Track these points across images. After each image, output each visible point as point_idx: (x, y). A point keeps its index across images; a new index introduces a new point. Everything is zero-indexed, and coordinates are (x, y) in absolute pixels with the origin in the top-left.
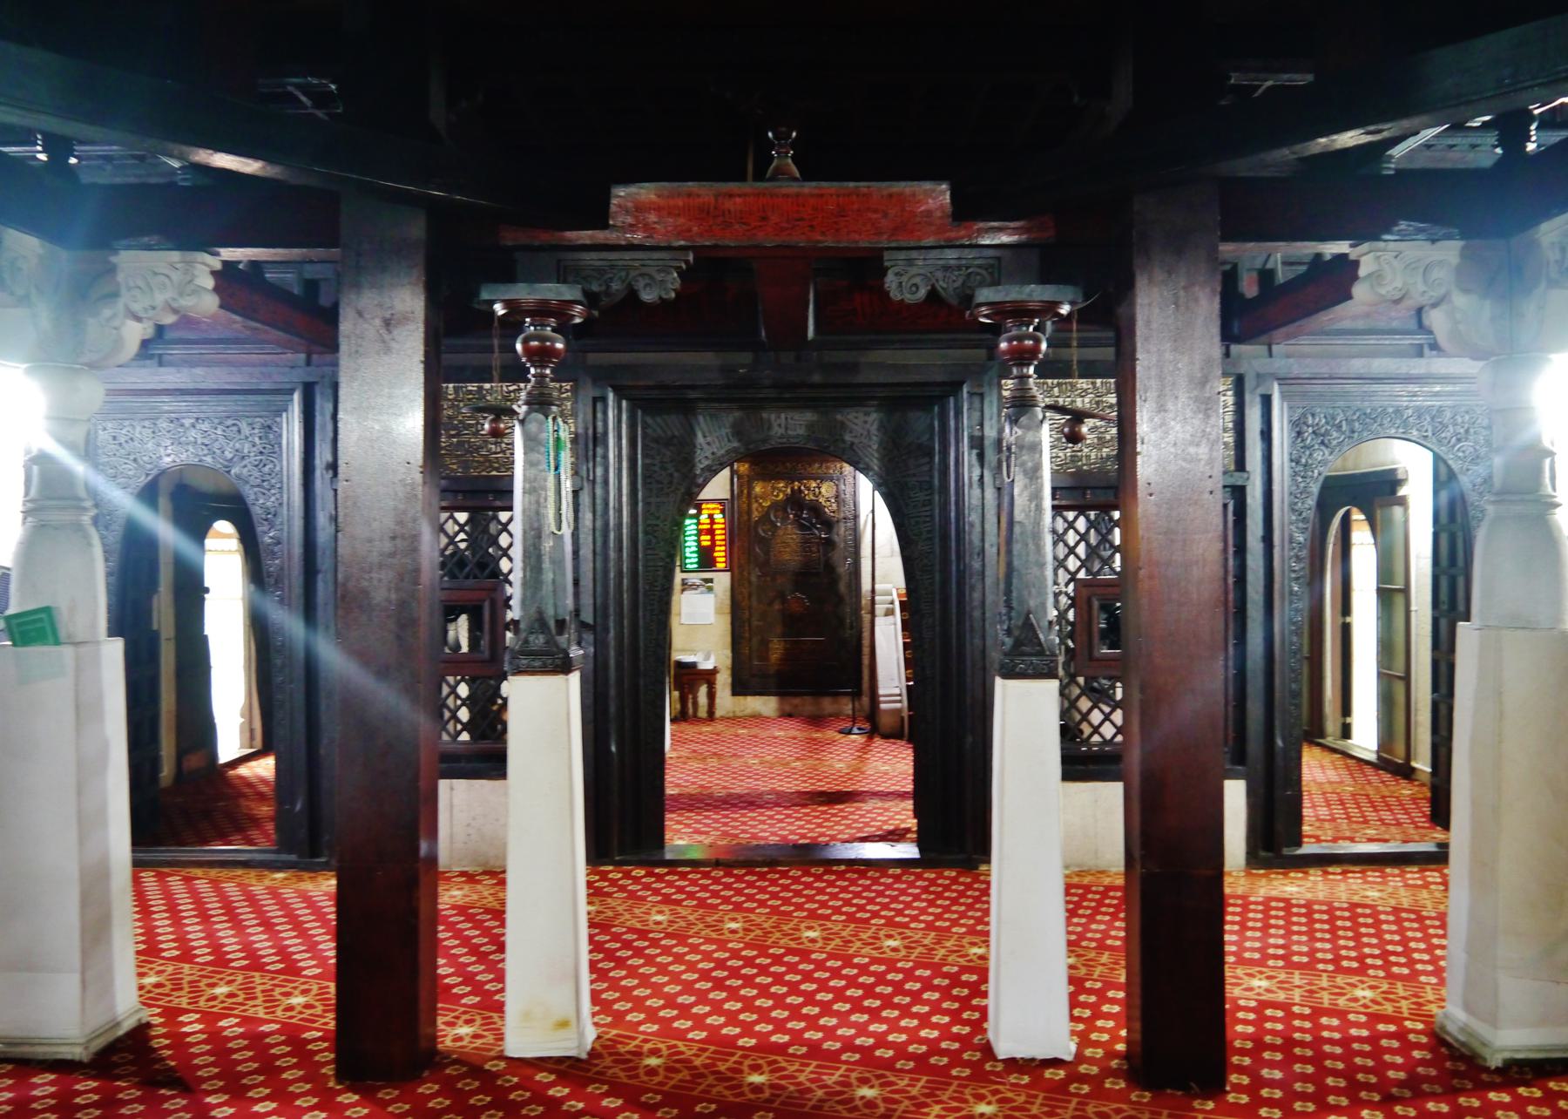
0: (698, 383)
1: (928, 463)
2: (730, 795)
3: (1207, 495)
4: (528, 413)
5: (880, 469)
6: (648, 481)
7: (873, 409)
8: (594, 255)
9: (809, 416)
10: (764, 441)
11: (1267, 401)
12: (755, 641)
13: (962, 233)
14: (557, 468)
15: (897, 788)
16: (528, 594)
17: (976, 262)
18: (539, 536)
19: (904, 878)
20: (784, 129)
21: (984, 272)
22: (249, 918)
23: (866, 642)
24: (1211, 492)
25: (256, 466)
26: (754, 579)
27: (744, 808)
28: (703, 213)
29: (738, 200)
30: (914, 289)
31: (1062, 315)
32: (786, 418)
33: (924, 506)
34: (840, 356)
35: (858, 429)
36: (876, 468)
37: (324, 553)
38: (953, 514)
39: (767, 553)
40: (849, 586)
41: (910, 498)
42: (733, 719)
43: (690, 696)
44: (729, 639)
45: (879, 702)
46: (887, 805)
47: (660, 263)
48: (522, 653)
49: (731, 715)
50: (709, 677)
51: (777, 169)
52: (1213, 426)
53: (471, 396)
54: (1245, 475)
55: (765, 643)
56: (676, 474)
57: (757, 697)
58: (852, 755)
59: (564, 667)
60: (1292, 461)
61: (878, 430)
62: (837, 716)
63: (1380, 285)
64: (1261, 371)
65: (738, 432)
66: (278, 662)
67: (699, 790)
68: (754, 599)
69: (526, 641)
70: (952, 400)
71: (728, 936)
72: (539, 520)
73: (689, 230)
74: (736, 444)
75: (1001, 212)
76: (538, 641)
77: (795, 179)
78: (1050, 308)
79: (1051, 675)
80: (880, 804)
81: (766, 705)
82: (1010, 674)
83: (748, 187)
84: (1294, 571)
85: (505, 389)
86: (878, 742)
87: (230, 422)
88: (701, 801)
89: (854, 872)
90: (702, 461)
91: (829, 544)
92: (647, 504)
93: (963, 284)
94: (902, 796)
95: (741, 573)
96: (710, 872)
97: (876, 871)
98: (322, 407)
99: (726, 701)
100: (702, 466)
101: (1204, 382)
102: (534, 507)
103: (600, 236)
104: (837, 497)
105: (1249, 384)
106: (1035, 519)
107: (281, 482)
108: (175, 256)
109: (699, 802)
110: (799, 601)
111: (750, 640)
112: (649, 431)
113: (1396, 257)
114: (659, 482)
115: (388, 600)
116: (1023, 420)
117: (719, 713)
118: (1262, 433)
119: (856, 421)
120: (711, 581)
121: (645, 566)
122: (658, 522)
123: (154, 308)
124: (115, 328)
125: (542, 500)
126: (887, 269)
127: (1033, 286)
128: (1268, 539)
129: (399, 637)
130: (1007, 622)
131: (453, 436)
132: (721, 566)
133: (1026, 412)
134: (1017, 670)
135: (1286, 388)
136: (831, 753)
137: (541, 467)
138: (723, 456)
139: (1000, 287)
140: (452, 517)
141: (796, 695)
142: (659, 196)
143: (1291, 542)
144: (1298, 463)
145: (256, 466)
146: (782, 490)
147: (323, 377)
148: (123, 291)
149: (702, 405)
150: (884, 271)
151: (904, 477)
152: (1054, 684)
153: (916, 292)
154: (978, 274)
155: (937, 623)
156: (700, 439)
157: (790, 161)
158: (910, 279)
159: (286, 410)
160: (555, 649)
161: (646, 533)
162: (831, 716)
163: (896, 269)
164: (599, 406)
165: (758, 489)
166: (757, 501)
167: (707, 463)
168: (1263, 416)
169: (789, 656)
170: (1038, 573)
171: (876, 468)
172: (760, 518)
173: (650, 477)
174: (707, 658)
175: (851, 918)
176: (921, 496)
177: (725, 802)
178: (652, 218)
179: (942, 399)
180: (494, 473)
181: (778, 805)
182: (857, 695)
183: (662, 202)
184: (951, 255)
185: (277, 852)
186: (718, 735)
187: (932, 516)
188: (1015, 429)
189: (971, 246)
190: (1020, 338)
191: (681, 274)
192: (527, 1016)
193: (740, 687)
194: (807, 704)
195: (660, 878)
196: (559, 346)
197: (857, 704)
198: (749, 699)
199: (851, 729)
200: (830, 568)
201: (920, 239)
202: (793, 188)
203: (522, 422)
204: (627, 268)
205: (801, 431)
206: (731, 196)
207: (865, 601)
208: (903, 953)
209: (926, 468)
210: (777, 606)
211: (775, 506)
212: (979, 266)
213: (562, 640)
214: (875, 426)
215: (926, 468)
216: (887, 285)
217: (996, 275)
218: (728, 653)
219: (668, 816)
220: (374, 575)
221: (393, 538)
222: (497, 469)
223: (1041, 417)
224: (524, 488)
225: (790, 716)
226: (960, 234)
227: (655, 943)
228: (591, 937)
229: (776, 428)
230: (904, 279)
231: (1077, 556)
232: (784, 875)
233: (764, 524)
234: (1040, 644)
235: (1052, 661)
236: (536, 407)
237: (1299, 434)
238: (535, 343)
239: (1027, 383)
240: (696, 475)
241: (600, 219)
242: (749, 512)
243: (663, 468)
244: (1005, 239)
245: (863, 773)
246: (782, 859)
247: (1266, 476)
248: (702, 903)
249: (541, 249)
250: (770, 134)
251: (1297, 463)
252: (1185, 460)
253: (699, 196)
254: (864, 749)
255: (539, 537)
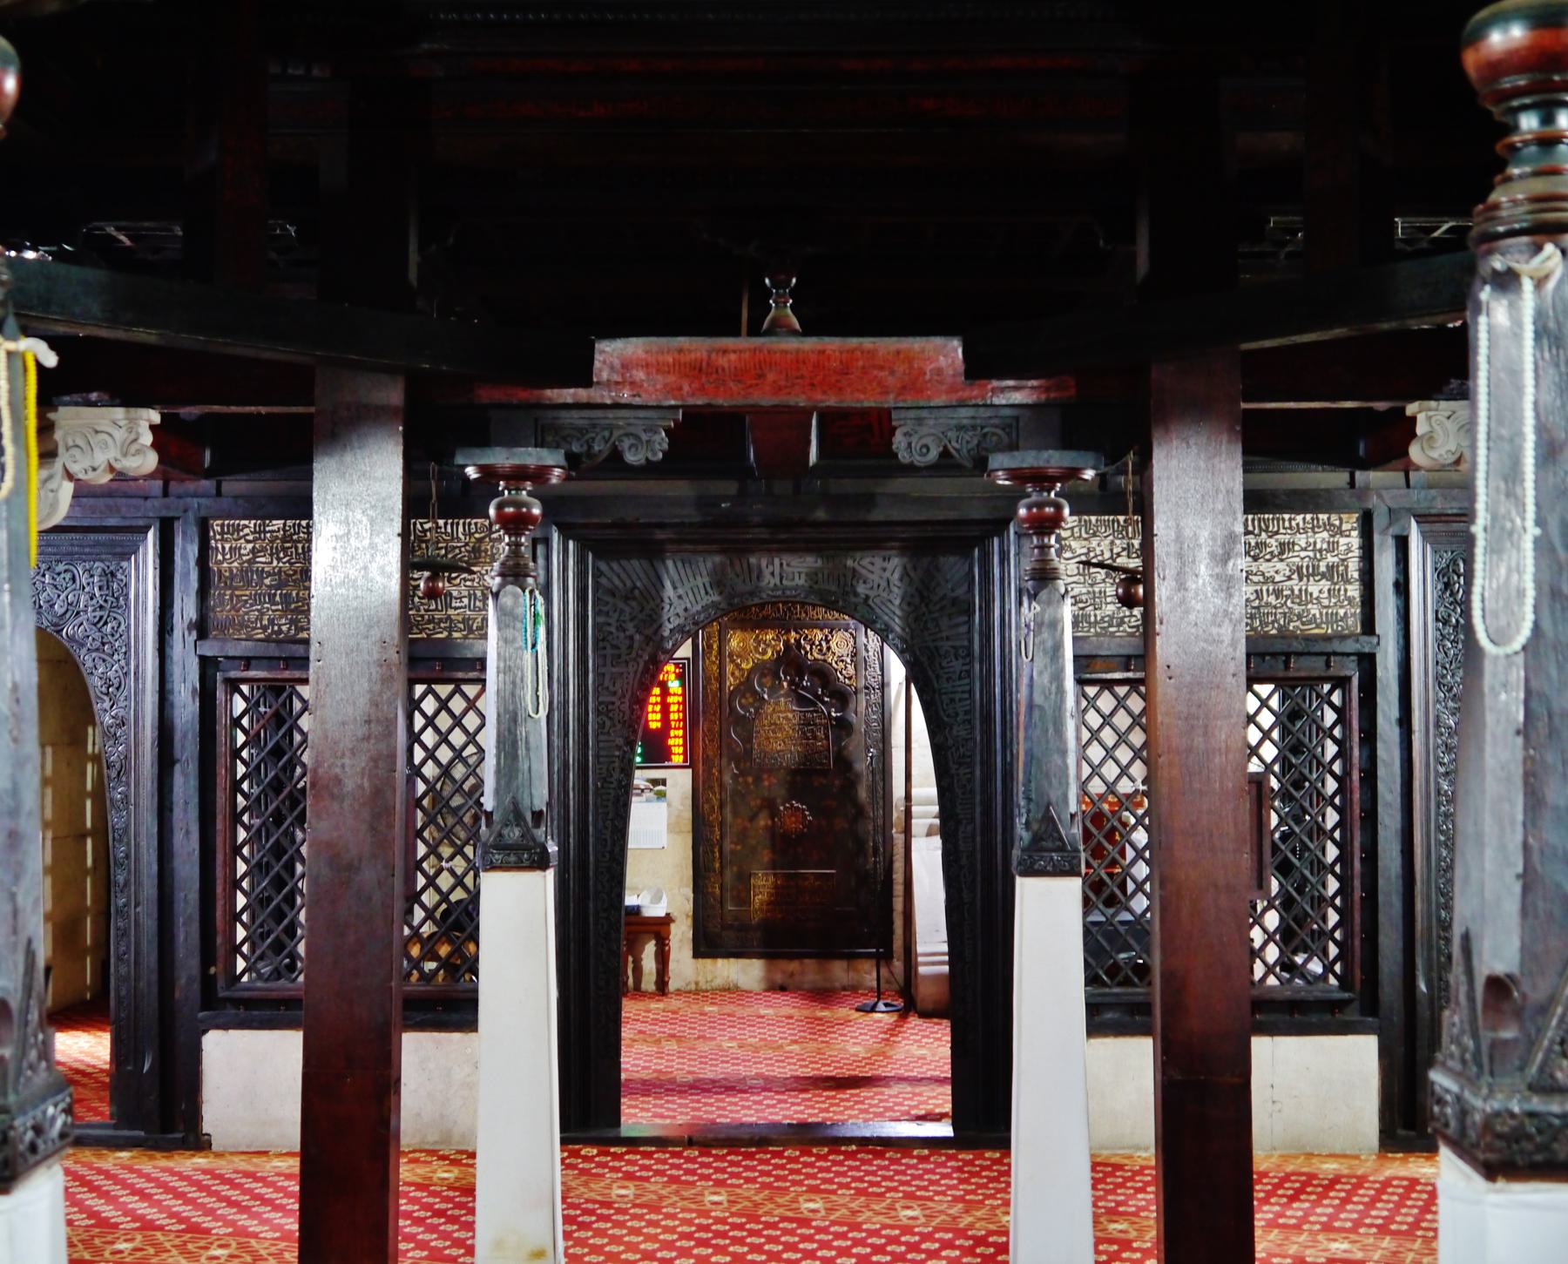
0: (667, 521)
1: (965, 623)
2: (700, 1080)
3: (1229, 679)
4: (502, 586)
5: (903, 629)
6: (601, 644)
7: (894, 552)
8: (575, 414)
9: (810, 562)
10: (752, 594)
11: (1402, 544)
12: (729, 875)
13: (975, 393)
14: (534, 646)
15: (937, 1073)
16: (503, 783)
17: (992, 422)
18: (514, 720)
19: (932, 1159)
20: (783, 277)
21: (1000, 432)
22: (117, 1190)
23: (898, 877)
24: (1234, 675)
25: (95, 625)
26: (727, 779)
27: (721, 1093)
28: (697, 370)
29: (733, 357)
30: (924, 450)
31: (1086, 480)
32: (781, 565)
33: (960, 678)
34: (848, 486)
35: (875, 578)
36: (898, 629)
38: (998, 690)
39: (748, 740)
40: (872, 790)
41: (942, 668)
42: (697, 993)
43: (630, 959)
44: (689, 872)
45: (917, 965)
46: (917, 1090)
47: (647, 422)
48: (496, 847)
49: (693, 987)
50: (659, 928)
51: (774, 322)
52: (1235, 606)
54: (1375, 640)
55: (744, 878)
56: (637, 637)
57: (732, 960)
58: (876, 1037)
59: (541, 863)
60: (1437, 619)
61: (901, 580)
62: (854, 989)
63: (1432, 448)
64: (1394, 506)
65: (718, 582)
66: (121, 879)
67: (655, 1075)
68: (728, 810)
69: (500, 835)
70: (996, 541)
71: (709, 1206)
72: (514, 703)
73: (680, 389)
74: (716, 598)
75: (1018, 371)
76: (514, 834)
77: (794, 333)
78: (1073, 473)
79: (1072, 872)
80: (909, 1089)
81: (746, 972)
82: (1025, 874)
83: (744, 343)
84: (1442, 764)
85: (418, 526)
86: (914, 1021)
87: (61, 567)
88: (655, 1086)
89: (869, 1152)
90: (671, 619)
91: (843, 726)
92: (599, 675)
93: (978, 445)
94: (939, 1081)
95: (708, 771)
96: (682, 1152)
97: (896, 1152)
98: (184, 550)
99: (684, 965)
100: (671, 626)
101: (1225, 558)
102: (509, 687)
103: (582, 394)
104: (854, 655)
105: (1379, 522)
106: (1055, 702)
107: (128, 645)
108: (119, 413)
109: (652, 1087)
110: (796, 815)
111: (721, 873)
112: (603, 581)
113: (1449, 418)
114: (616, 647)
115: (361, 787)
116: (1043, 595)
117: (673, 985)
118: (1397, 585)
119: (870, 567)
120: (663, 782)
121: (597, 756)
122: (613, 699)
123: (94, 469)
124: (52, 491)
125: (518, 681)
126: (895, 429)
127: (1051, 452)
128: (1405, 721)
129: (373, 828)
130: (1025, 816)
132: (677, 759)
133: (1045, 586)
134: (1036, 867)
135: (1427, 527)
136: (845, 1035)
137: (517, 645)
138: (698, 613)
139: (1016, 453)
141: (791, 957)
142: (647, 352)
143: (1437, 725)
144: (1446, 622)
145: (95, 625)
146: (770, 644)
147: (185, 511)
148: (61, 450)
149: (669, 547)
150: (893, 431)
151: (934, 641)
152: (1076, 883)
153: (925, 455)
154: (994, 434)
155: (978, 831)
156: (669, 591)
157: (789, 311)
158: (921, 438)
159: (135, 552)
160: (531, 843)
161: (598, 713)
162: (844, 989)
163: (904, 429)
164: (540, 549)
165: (735, 642)
166: (733, 661)
167: (676, 622)
168: (1398, 563)
169: (781, 897)
170: (1059, 762)
171: (898, 629)
172: (737, 688)
173: (603, 640)
174: (657, 899)
175: (860, 1192)
176: (957, 665)
177: (692, 1087)
178: (640, 375)
179: (983, 541)
181: (769, 1090)
182: (884, 957)
183: (652, 359)
184: (964, 413)
185: (115, 1127)
186: (674, 1012)
187: (971, 692)
188: (1034, 604)
189: (985, 406)
190: (1040, 505)
191: (668, 431)
192: (499, 1245)
193: (706, 945)
194: (808, 972)
195: (617, 1157)
196: (536, 511)
197: (884, 971)
198: (720, 962)
199: (875, 1005)
200: (844, 764)
201: (929, 399)
202: (792, 344)
203: (496, 595)
204: (611, 428)
205: (801, 581)
206: (725, 352)
207: (897, 813)
208: (923, 1220)
209: (963, 629)
210: (763, 821)
211: (759, 668)
212: (997, 426)
213: (540, 833)
214: (897, 575)
215: (963, 629)
216: (894, 447)
217: (1014, 435)
218: (689, 892)
219: (622, 1100)
220: (347, 761)
221: (368, 722)
223: (1062, 590)
224: (498, 668)
225: (783, 989)
226: (973, 393)
227: (620, 1211)
228: (563, 1160)
229: (767, 578)
230: (914, 440)
231: (423, 714)
232: (779, 1155)
233: (743, 696)
234: (1061, 838)
235: (1074, 858)
236: (510, 579)
237: (1447, 585)
238: (510, 510)
239: (1048, 554)
240: (663, 637)
241: (586, 380)
242: (721, 678)
243: (621, 629)
244: (1018, 397)
245: (886, 1057)
246: (775, 1137)
247: (1401, 641)
248: (674, 1180)
249: (518, 407)
250: (767, 281)
251: (1444, 624)
252: (1206, 641)
253: (690, 351)
254: (893, 1031)
255: (515, 721)
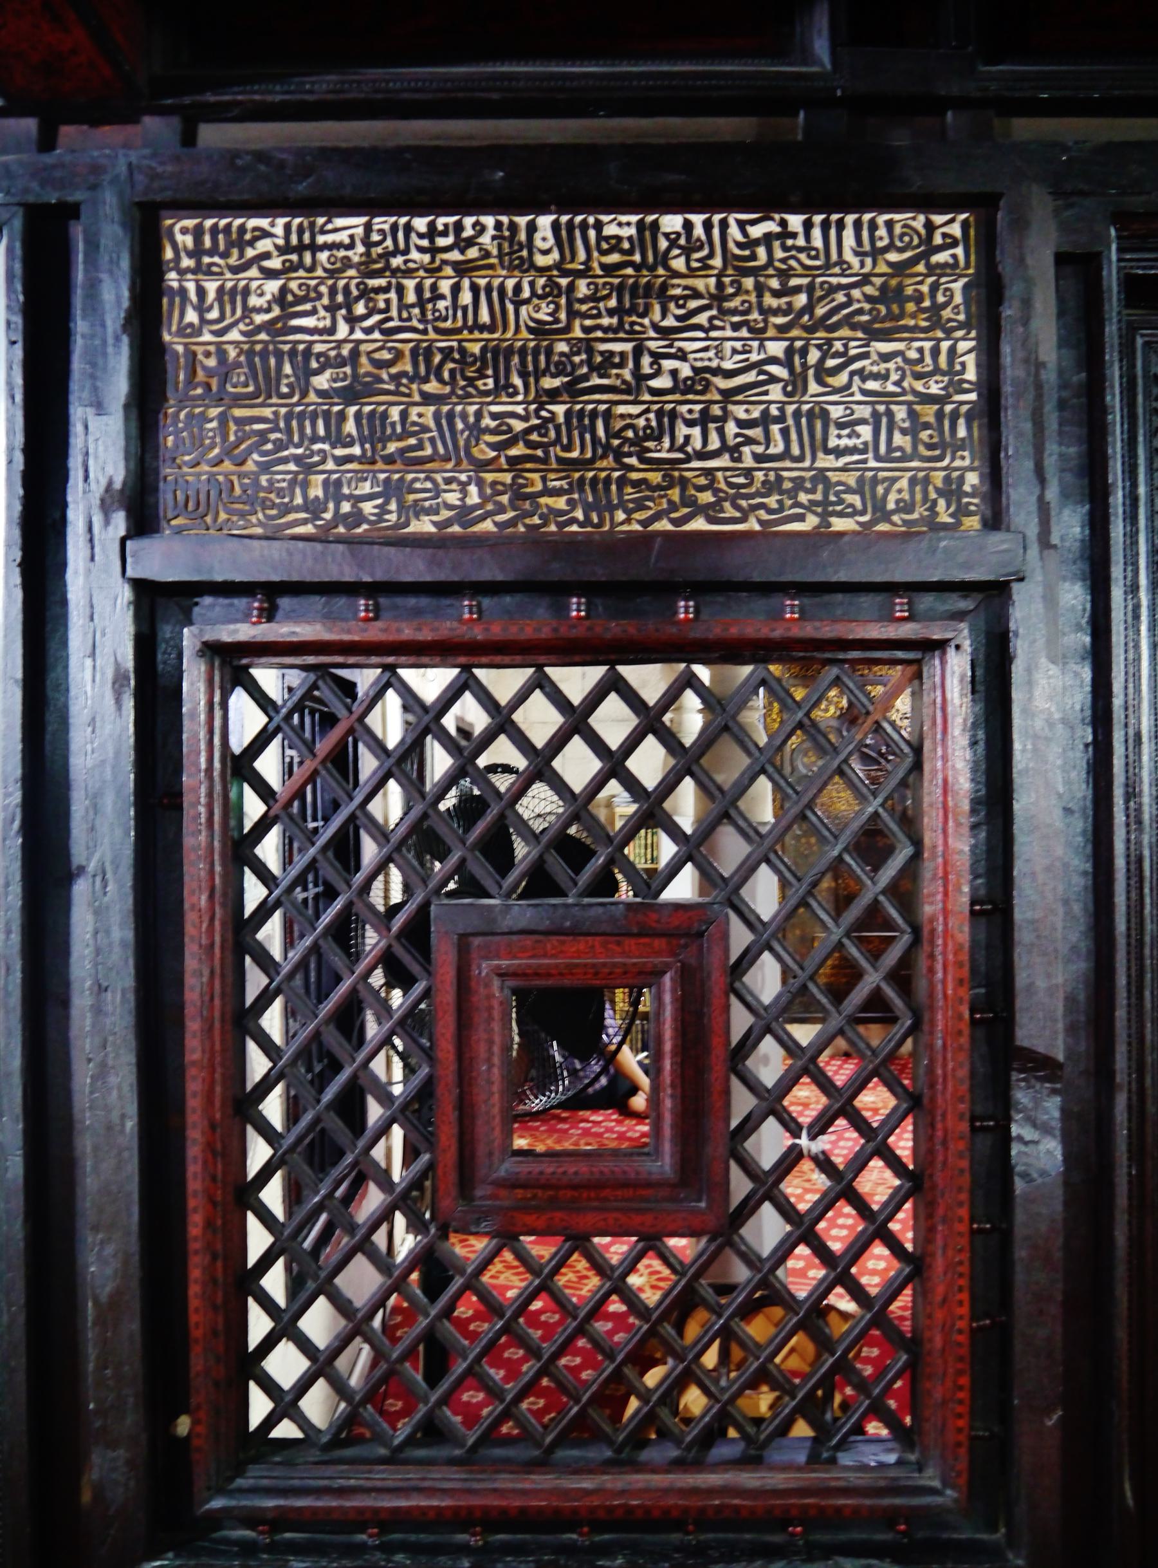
37: (95, 808)
53: (615, 258)
85: (734, 232)
131: (553, 395)
140: (541, 683)
180: (699, 524)
222: (711, 512)
